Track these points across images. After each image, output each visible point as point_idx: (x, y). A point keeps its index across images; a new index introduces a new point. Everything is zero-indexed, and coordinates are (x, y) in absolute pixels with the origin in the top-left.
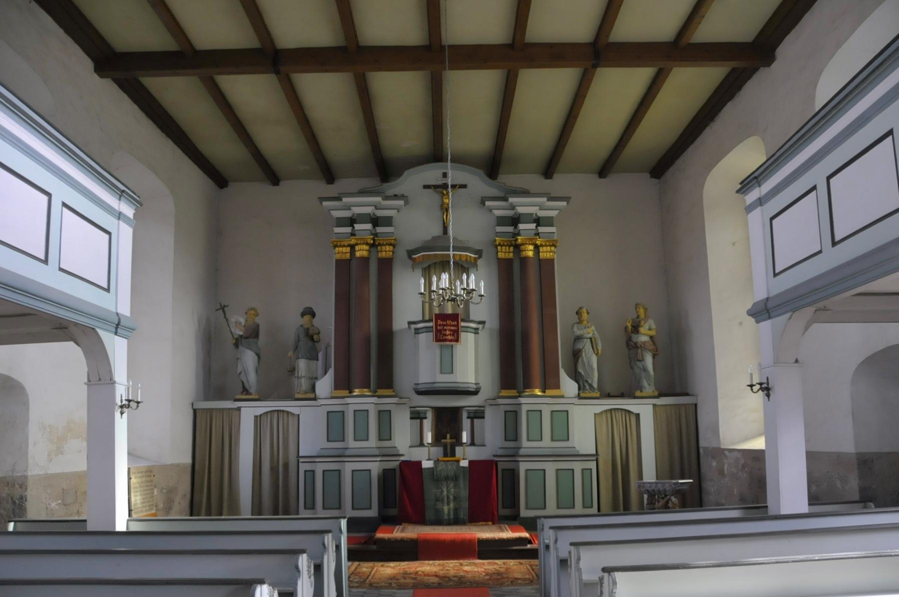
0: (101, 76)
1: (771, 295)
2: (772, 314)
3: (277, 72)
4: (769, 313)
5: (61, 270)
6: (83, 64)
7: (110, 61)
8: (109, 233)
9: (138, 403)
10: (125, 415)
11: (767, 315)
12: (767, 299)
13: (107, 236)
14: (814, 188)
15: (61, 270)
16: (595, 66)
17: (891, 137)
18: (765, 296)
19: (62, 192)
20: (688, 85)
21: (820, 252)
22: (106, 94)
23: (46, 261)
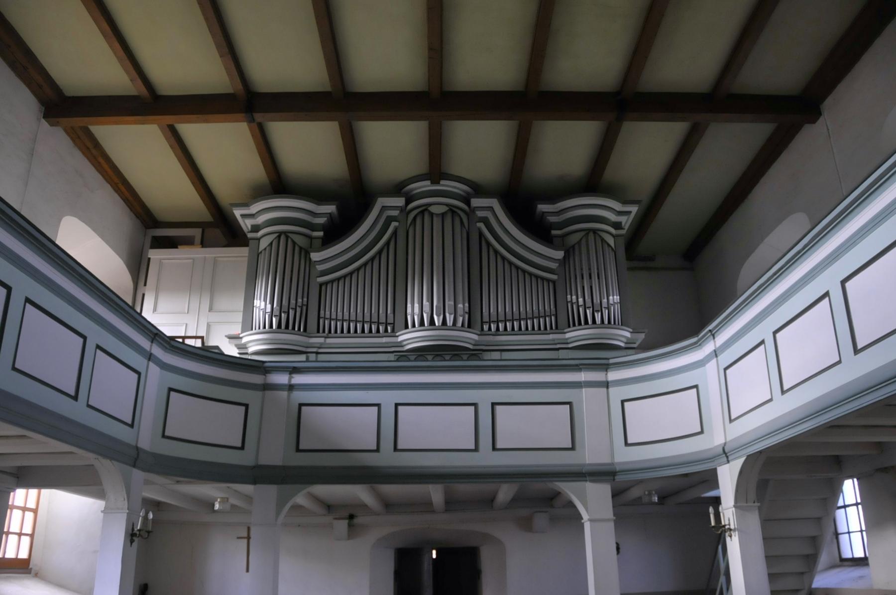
0: (52, 125)
1: (728, 440)
2: (730, 458)
3: (251, 120)
4: (727, 457)
5: (89, 406)
6: (23, 103)
7: (61, 106)
8: (139, 374)
9: (149, 532)
10: (135, 544)
11: (725, 459)
12: (725, 444)
13: (136, 376)
14: (763, 342)
15: (89, 406)
16: (620, 120)
17: (827, 299)
18: (723, 441)
19: (96, 334)
20: (729, 144)
21: (771, 400)
22: (55, 141)
23: (75, 398)
